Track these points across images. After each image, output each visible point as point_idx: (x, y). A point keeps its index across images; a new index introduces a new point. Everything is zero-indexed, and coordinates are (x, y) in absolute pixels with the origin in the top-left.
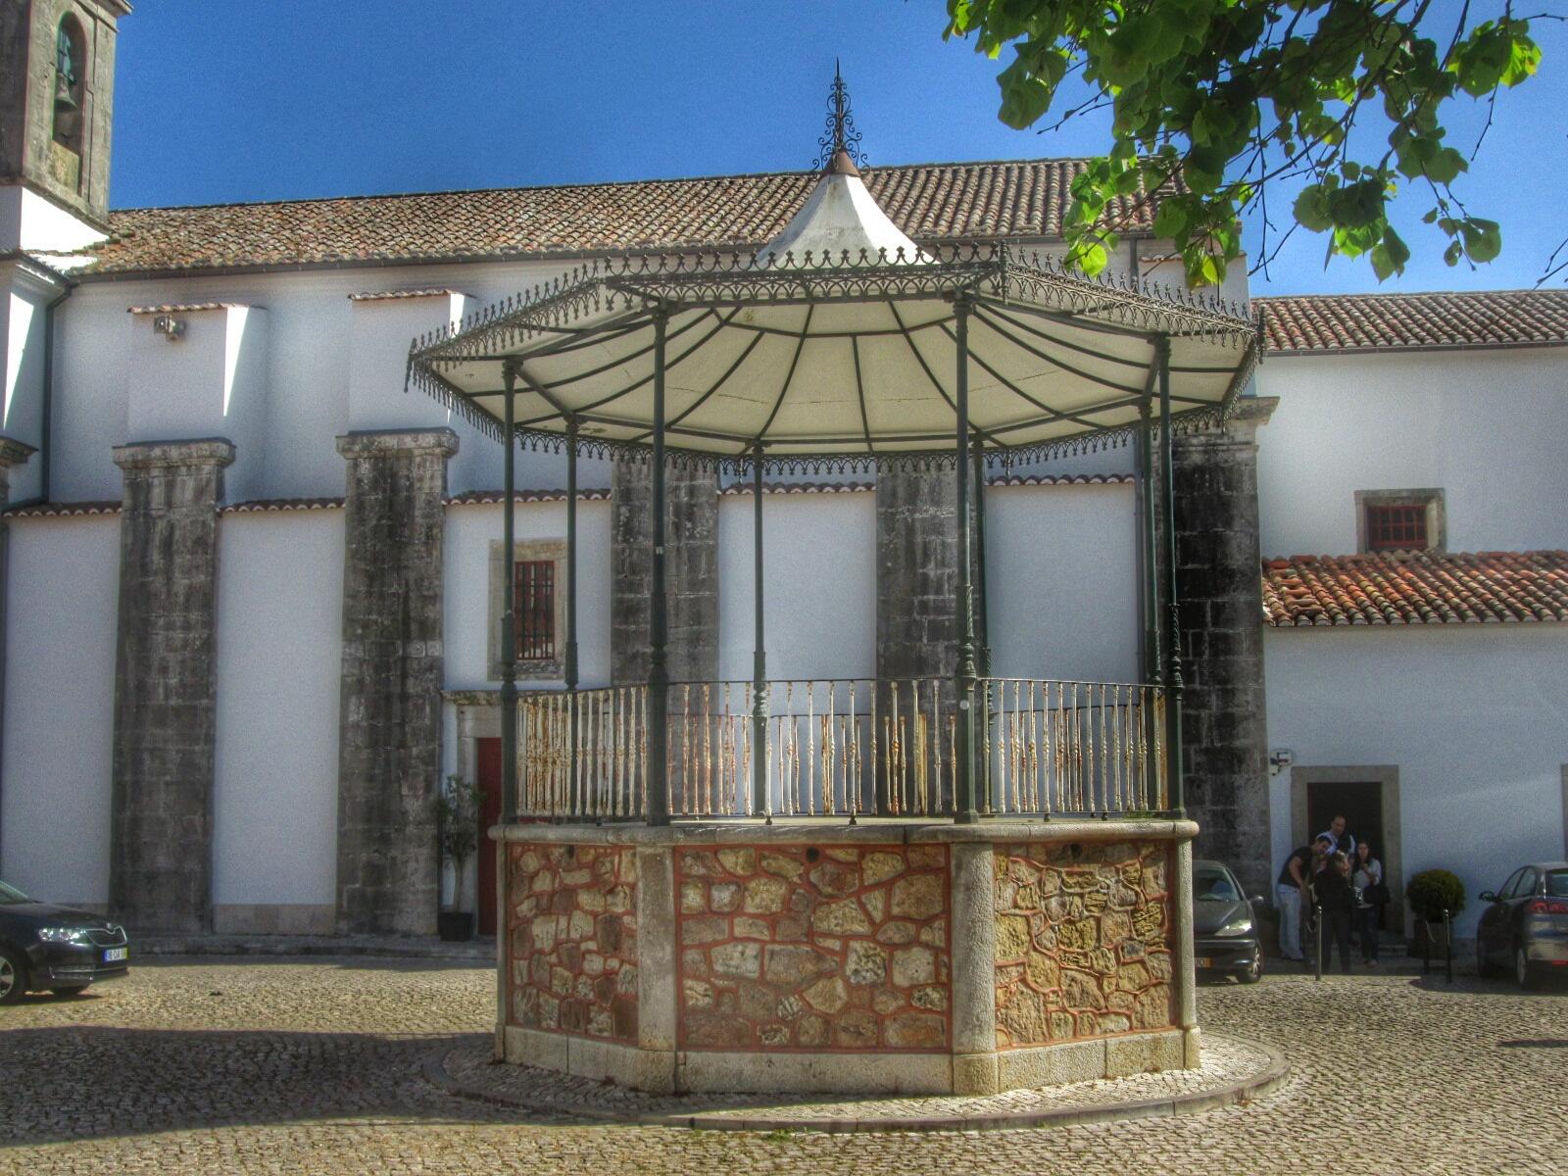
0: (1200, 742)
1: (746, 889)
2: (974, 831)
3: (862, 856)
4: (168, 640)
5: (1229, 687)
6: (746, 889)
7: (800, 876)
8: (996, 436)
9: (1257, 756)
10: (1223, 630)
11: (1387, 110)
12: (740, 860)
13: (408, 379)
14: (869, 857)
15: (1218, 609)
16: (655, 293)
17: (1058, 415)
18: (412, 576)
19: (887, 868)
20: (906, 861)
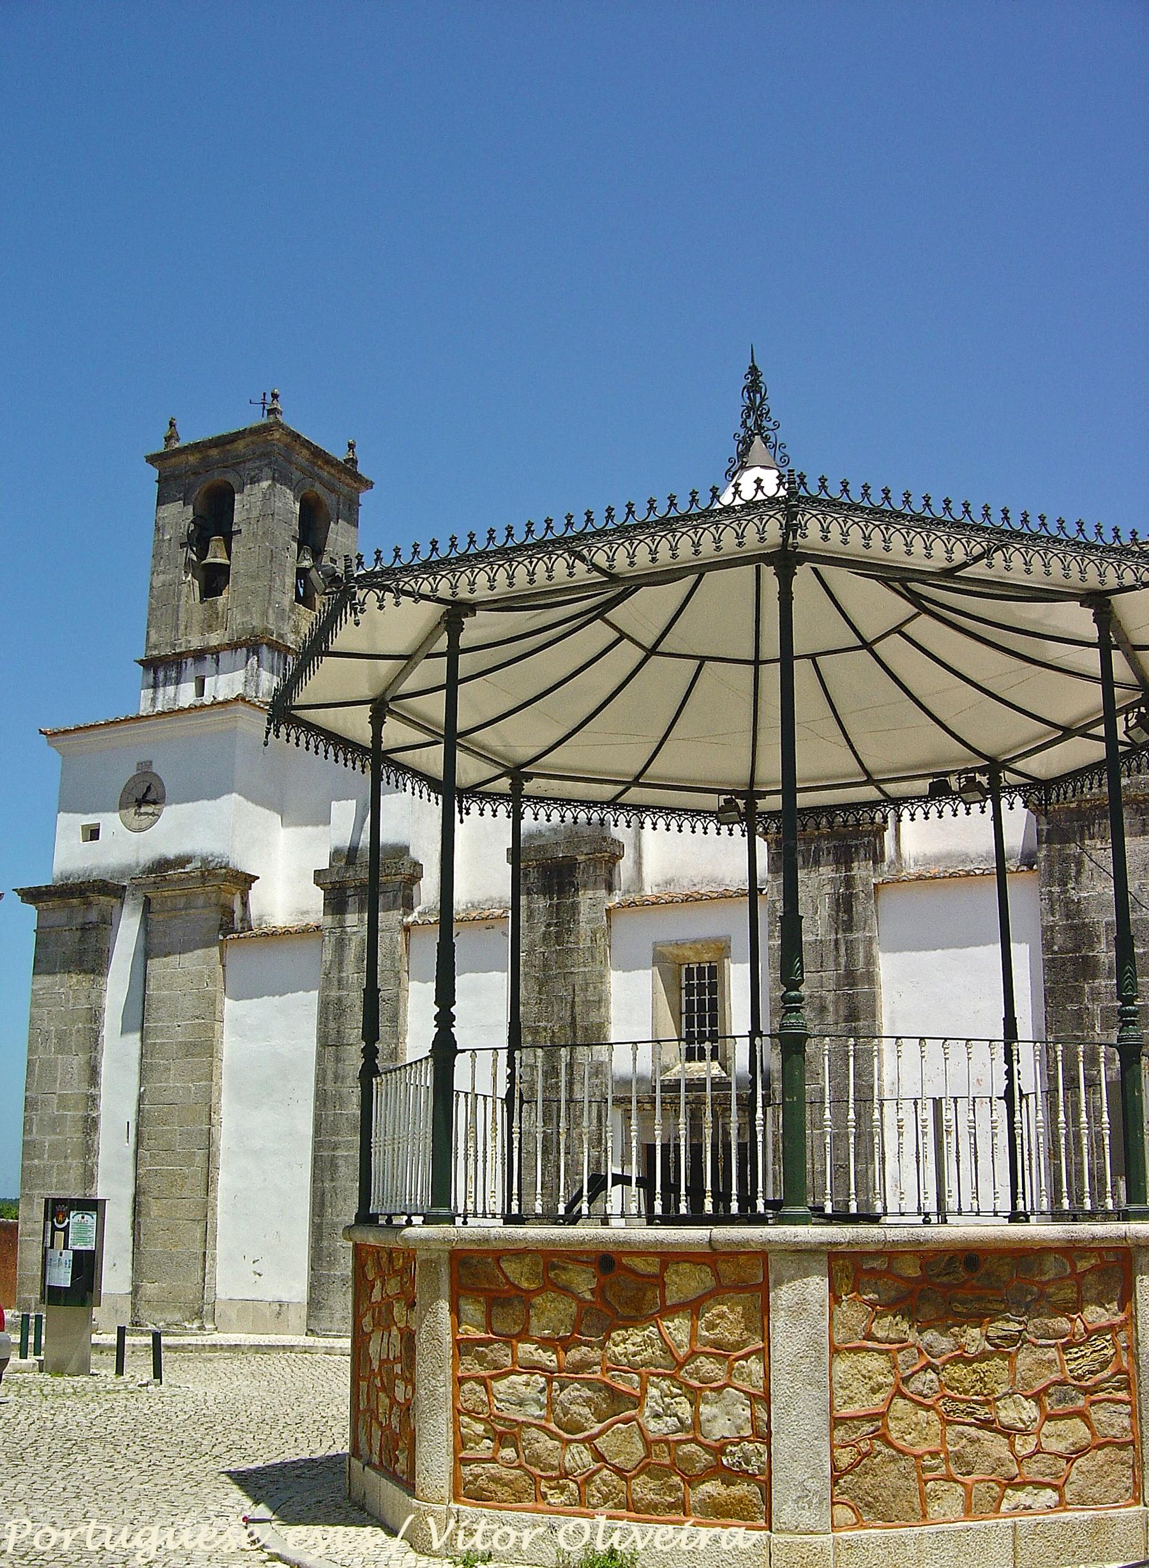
1: (532, 1306)
3: (664, 1266)
6: (532, 1306)
7: (592, 1291)
8: (1019, 765)
12: (525, 1270)
13: (268, 733)
14: (672, 1268)
16: (407, 588)
17: (1067, 732)
18: (579, 980)
19: (693, 1284)
20: (716, 1275)
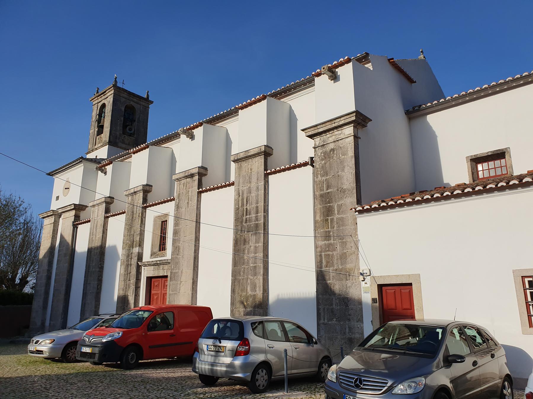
0: (333, 266)
2: (217, 370)
4: (104, 239)
5: (344, 240)
9: (356, 272)
10: (342, 216)
11: (296, 120)
15: (340, 207)
